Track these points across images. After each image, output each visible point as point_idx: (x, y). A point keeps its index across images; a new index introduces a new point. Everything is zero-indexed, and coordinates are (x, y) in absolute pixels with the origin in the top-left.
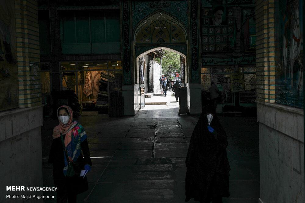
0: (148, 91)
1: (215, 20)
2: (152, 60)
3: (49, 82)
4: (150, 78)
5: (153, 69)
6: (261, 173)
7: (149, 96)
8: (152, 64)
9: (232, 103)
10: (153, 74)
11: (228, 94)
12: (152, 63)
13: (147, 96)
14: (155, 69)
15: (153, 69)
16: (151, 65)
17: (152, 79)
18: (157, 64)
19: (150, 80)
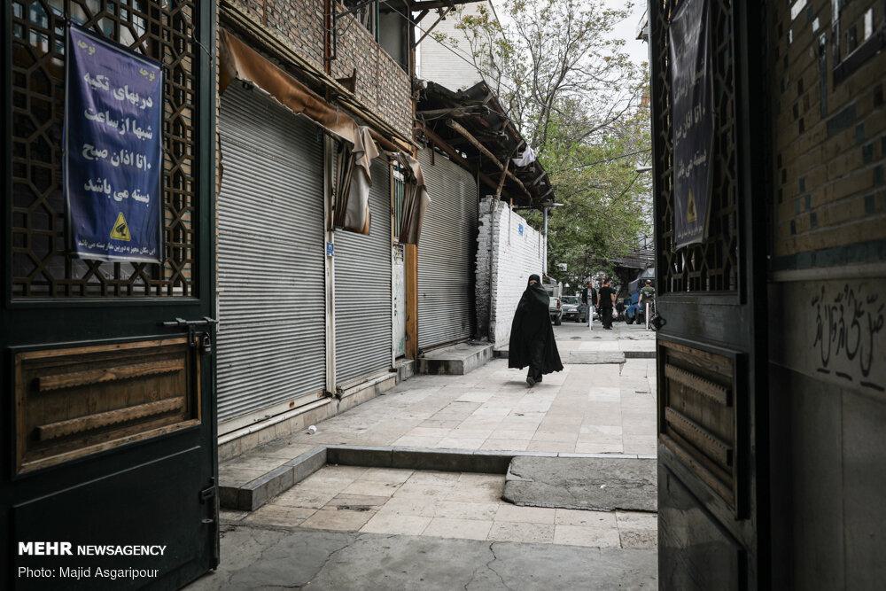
0: (472, 337)
1: (666, 466)
2: (490, 199)
3: (102, 380)
4: (478, 277)
5: (491, 234)
6: (655, 378)
7: (453, 367)
8: (491, 213)
9: (158, 279)
10: (491, 257)
11: (523, 149)
12: (492, 207)
13: (442, 369)
14: (502, 236)
15: (491, 234)
16: (485, 219)
17: (490, 282)
18: (518, 220)
19: (480, 285)
